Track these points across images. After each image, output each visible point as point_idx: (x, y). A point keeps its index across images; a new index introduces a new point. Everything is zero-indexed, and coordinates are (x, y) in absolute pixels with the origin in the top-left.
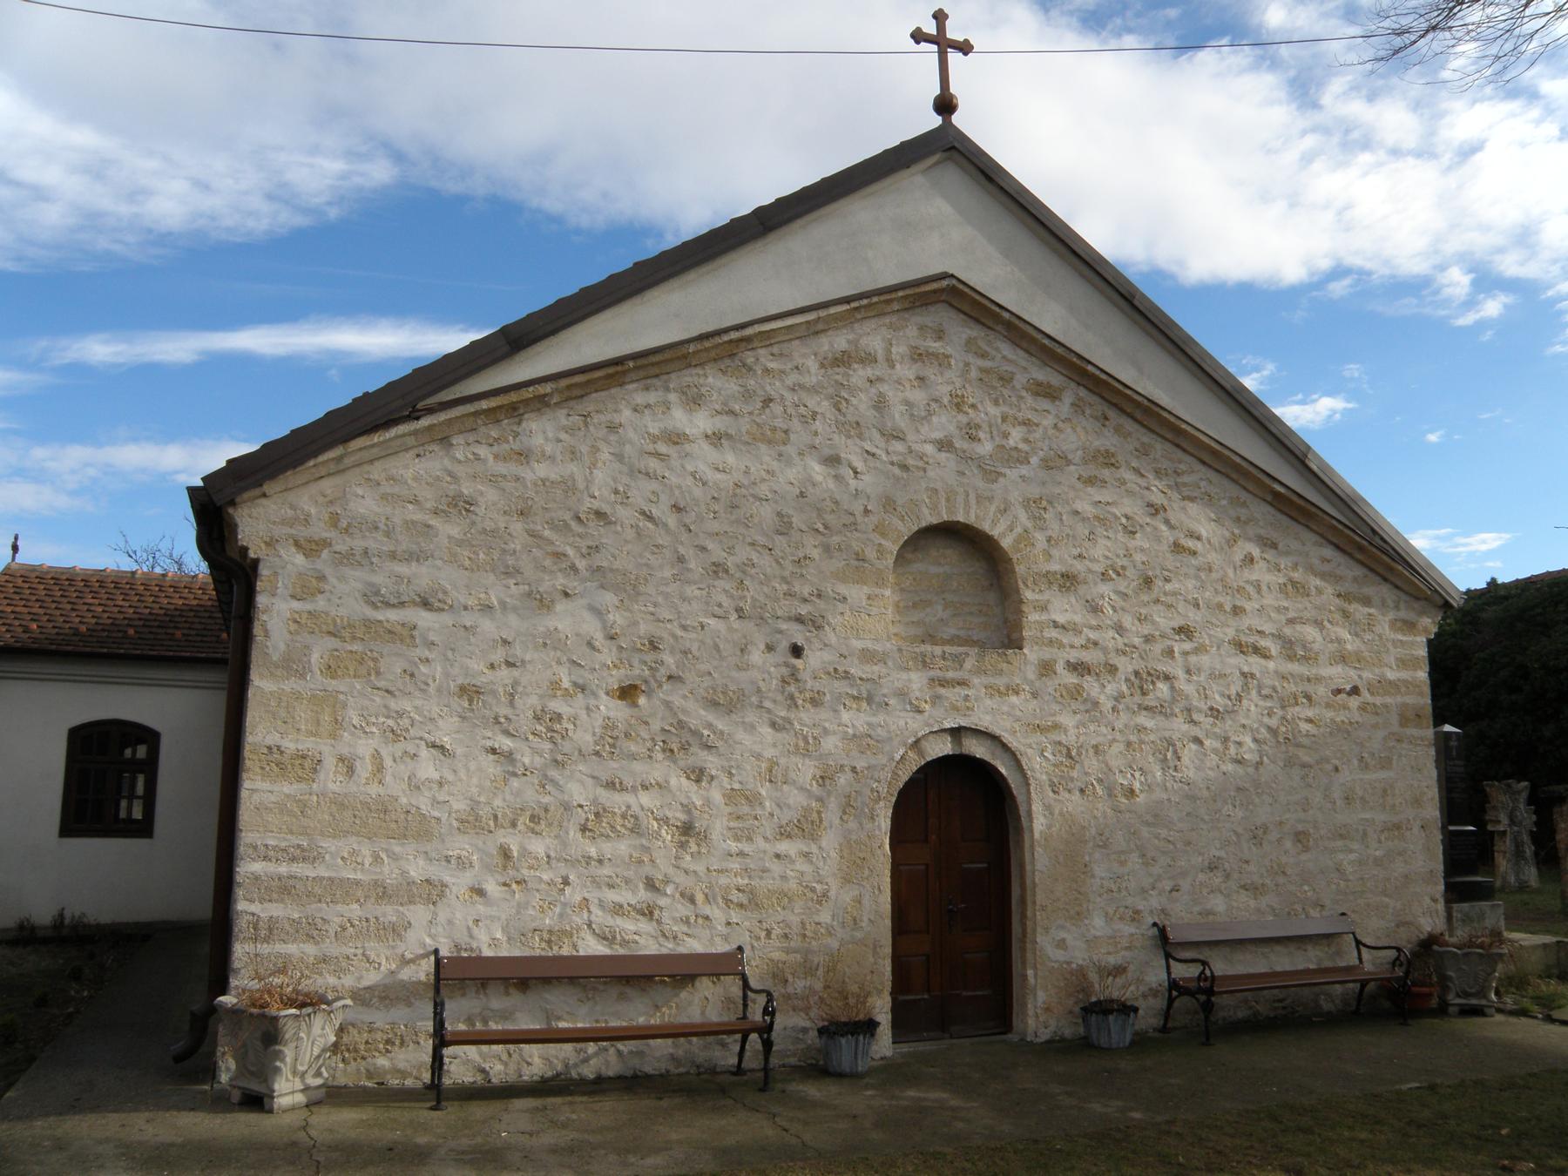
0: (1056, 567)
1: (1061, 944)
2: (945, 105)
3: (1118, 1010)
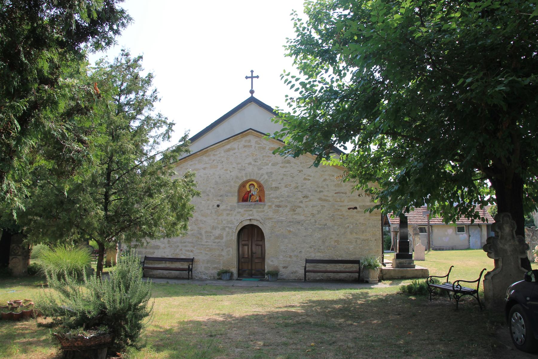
0: (273, 186)
2: (252, 92)
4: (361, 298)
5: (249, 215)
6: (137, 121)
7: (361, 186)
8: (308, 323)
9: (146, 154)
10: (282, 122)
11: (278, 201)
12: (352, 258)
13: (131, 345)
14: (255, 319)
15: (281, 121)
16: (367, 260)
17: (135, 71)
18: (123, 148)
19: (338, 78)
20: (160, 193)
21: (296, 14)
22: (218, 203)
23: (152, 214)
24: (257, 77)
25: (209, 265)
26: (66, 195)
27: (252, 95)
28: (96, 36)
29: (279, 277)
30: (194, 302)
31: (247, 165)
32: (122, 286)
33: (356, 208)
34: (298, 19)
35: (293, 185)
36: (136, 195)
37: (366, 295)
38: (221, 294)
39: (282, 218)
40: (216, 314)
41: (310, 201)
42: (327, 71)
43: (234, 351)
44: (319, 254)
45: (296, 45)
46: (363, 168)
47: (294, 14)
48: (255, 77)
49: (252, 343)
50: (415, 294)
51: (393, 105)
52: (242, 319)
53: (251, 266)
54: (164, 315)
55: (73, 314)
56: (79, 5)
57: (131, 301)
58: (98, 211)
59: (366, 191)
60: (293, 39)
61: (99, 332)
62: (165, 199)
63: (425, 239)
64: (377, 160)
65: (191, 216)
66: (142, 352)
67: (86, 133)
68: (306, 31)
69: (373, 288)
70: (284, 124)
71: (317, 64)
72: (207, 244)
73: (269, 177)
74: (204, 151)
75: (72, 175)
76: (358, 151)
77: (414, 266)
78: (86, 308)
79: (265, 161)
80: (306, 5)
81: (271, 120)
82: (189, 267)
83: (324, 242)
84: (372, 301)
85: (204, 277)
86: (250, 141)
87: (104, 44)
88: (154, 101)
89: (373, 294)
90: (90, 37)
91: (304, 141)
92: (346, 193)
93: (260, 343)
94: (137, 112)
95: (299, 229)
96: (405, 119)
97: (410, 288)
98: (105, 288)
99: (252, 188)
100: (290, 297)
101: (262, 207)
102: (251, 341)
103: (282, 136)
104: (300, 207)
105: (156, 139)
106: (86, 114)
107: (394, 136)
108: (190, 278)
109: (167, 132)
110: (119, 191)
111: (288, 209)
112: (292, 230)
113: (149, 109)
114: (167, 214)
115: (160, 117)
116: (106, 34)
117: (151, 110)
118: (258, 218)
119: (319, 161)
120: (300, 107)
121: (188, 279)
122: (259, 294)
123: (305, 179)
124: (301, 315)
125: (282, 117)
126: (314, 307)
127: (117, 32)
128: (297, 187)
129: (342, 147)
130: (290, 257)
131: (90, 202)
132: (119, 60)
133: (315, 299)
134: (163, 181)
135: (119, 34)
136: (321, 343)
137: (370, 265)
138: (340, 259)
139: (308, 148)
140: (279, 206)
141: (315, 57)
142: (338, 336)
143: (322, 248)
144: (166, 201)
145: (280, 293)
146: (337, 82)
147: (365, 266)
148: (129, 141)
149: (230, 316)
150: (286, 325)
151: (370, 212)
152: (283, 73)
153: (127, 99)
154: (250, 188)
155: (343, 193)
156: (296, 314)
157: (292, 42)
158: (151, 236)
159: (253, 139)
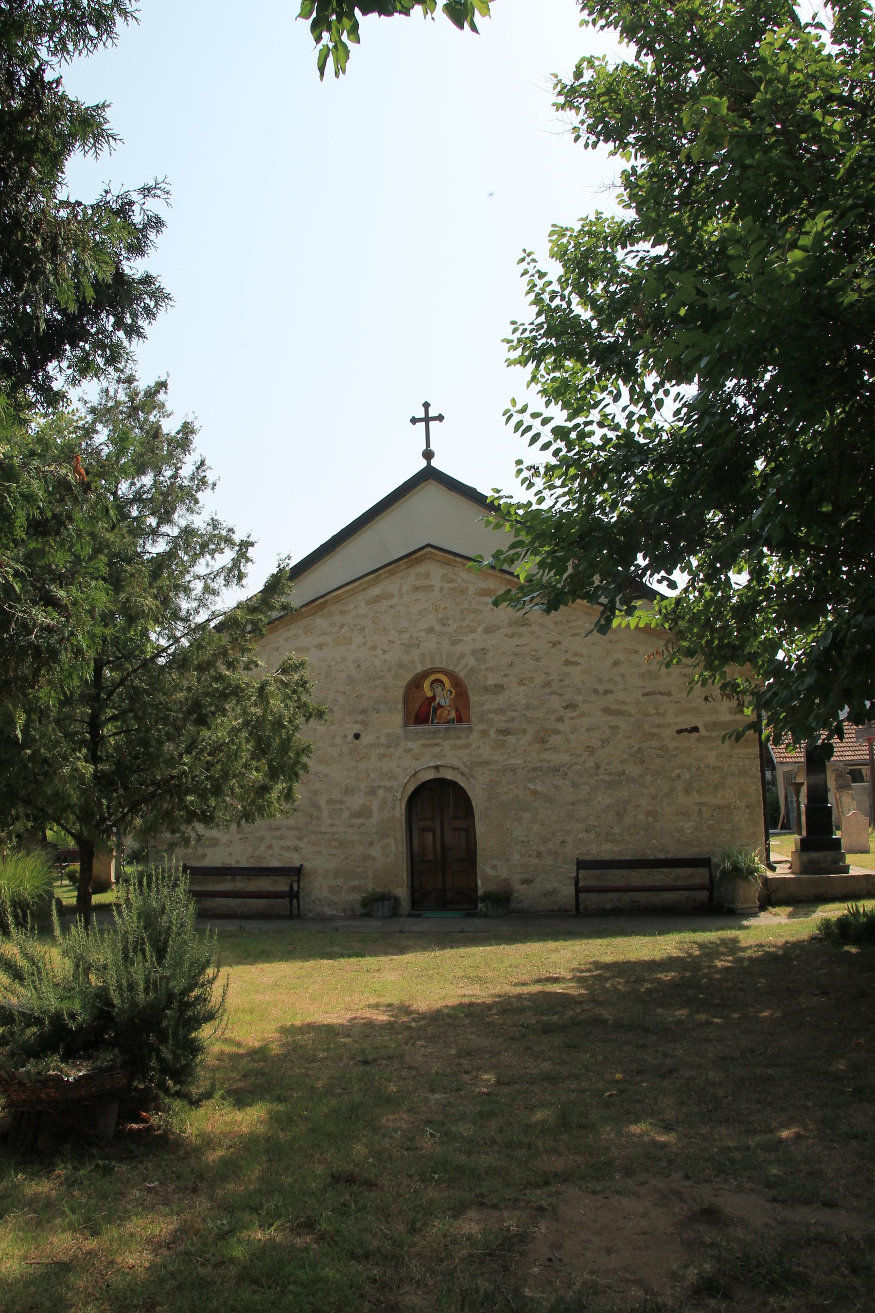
0: (490, 682)
1: (494, 867)
2: (428, 455)
3: (633, 232)
4: (724, 954)
5: (434, 756)
6: (160, 540)
7: (710, 677)
8: (598, 1021)
9: (186, 620)
10: (511, 526)
11: (503, 718)
12: (691, 852)
13: (178, 1095)
14: (467, 1016)
15: (508, 524)
16: (729, 857)
17: (152, 418)
18: (130, 608)
19: (644, 412)
20: (224, 712)
21: (534, 261)
22: (357, 728)
23: (209, 766)
24: (440, 418)
25: (340, 882)
26: (20, 736)
27: (429, 463)
28: (81, 344)
29: (513, 905)
30: (310, 976)
31: (423, 634)
32: (147, 947)
33: (695, 729)
34: (538, 271)
35: (539, 679)
36: (165, 720)
37: (732, 946)
38: (374, 953)
39: (514, 761)
40: (369, 1006)
41: (582, 715)
42: (617, 398)
43: (426, 1101)
44: (609, 846)
45: (535, 337)
46: (713, 630)
47: (528, 259)
48: (420, 420)
49: (466, 1078)
50: (856, 942)
51: (794, 475)
52: (436, 1017)
53: (442, 882)
54: (243, 1011)
55: (30, 1019)
56: (55, 273)
57: (171, 984)
58: (80, 764)
59: (723, 687)
60: (527, 323)
61: (99, 1063)
62: (240, 730)
63: (865, 797)
64: (747, 608)
65: (305, 767)
66: (202, 1111)
67: (62, 580)
68: (557, 301)
69: (747, 927)
70: (517, 533)
71: (591, 381)
72: (334, 829)
73: (477, 660)
74: (317, 605)
75: (33, 687)
76: (701, 591)
77: (846, 869)
78: (65, 1005)
79: (466, 622)
80: (554, 237)
81: (484, 522)
82: (291, 888)
83: (620, 816)
84: (750, 959)
85: (328, 911)
86: (428, 575)
87: (100, 361)
88: (199, 489)
89: (751, 942)
90: (67, 347)
91: (570, 570)
92: (669, 694)
93: (486, 1077)
94: (160, 518)
95: (557, 787)
96: (824, 509)
97: (843, 923)
98: (103, 953)
99: (438, 690)
100: (545, 955)
101: (463, 735)
102: (466, 1072)
103: (512, 561)
104: (558, 732)
105: (209, 581)
106: (58, 533)
107: (789, 549)
108: (294, 915)
109: (236, 563)
110: (124, 712)
111: (528, 737)
112: (539, 789)
113: (190, 510)
114: (246, 766)
115: (215, 527)
116: (107, 337)
117: (192, 512)
118: (455, 762)
119: (609, 621)
120: (552, 487)
121: (290, 917)
122: (468, 950)
123: (567, 663)
124: (581, 1003)
125: (509, 513)
126: (607, 979)
127: (133, 331)
128: (547, 684)
129: (665, 583)
130: (539, 855)
131: (57, 743)
132: (112, 393)
133: (608, 959)
134: (229, 684)
135: (141, 335)
136: (640, 1072)
137: (736, 869)
138: (662, 856)
139: (578, 588)
140: (505, 732)
141: (584, 364)
142: (679, 1053)
143: (616, 830)
144: (244, 734)
145: (520, 946)
146: (641, 424)
147: (724, 872)
148: (145, 590)
149: (405, 1010)
150: (547, 1030)
151: (737, 739)
152: (510, 407)
153: (133, 488)
154: (432, 689)
155: (661, 693)
156: (565, 1000)
157: (524, 331)
158: (207, 819)
159: (435, 572)
